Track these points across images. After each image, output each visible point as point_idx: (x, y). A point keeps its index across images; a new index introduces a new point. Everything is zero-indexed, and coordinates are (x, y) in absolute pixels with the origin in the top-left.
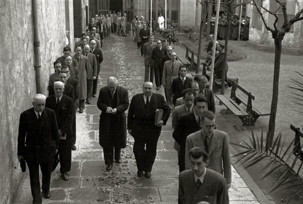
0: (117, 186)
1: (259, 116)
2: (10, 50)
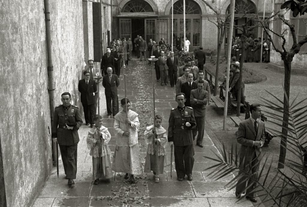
0: (125, 206)
1: (272, 137)
2: (22, 74)
